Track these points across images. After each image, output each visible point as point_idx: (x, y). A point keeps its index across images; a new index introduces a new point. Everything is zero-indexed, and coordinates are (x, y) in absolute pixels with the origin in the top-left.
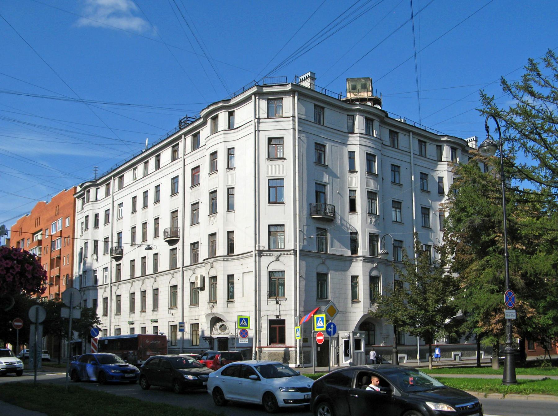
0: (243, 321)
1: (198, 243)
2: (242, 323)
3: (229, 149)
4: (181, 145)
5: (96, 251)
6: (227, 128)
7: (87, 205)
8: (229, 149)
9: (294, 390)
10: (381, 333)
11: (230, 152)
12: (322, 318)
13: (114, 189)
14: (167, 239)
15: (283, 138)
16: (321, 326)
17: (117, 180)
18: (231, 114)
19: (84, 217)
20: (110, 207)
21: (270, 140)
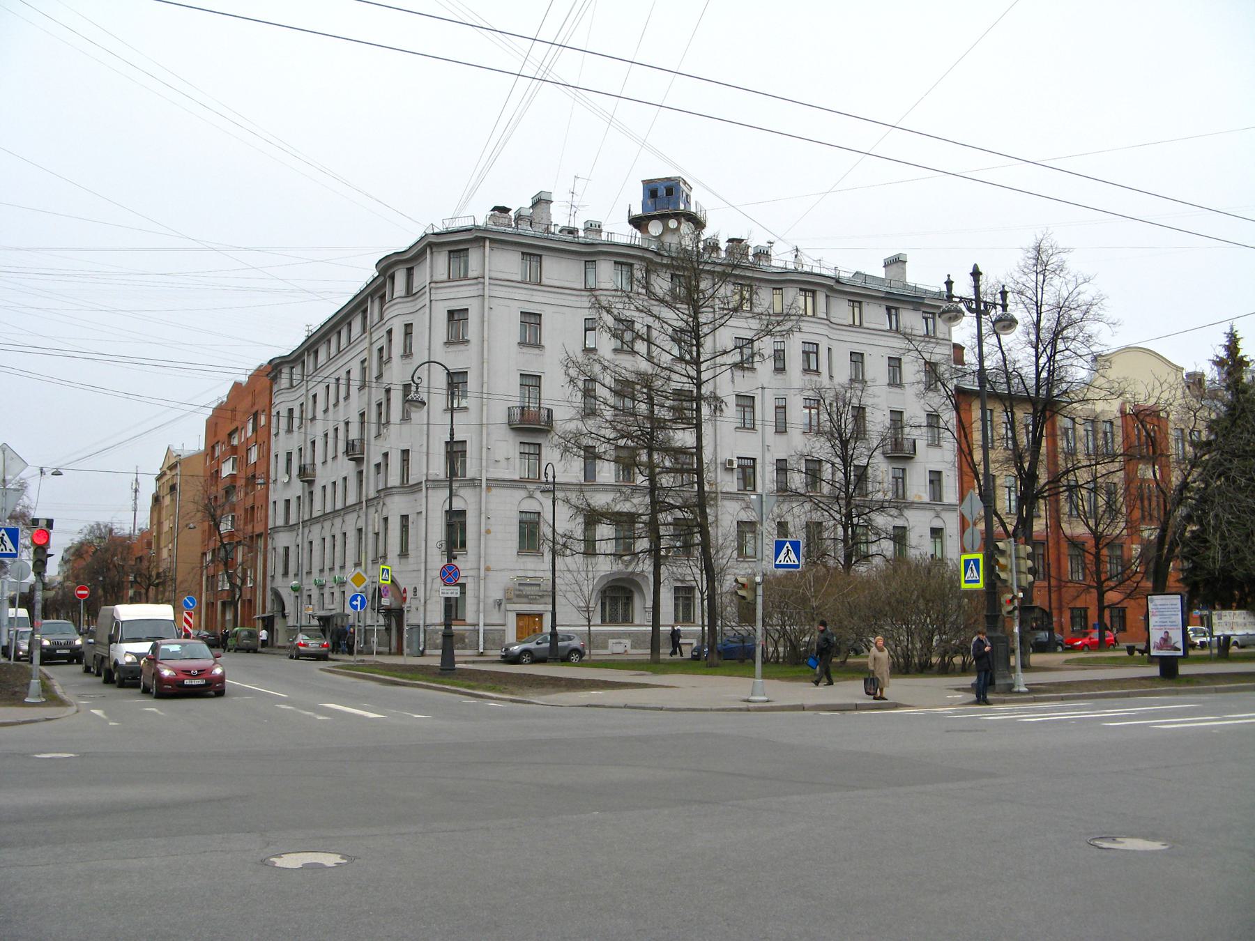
0: (785, 550)
2: (782, 556)
7: (400, 303)
9: (58, 652)
10: (313, 617)
12: (976, 561)
15: (467, 310)
16: (974, 579)
18: (410, 272)
21: (451, 313)
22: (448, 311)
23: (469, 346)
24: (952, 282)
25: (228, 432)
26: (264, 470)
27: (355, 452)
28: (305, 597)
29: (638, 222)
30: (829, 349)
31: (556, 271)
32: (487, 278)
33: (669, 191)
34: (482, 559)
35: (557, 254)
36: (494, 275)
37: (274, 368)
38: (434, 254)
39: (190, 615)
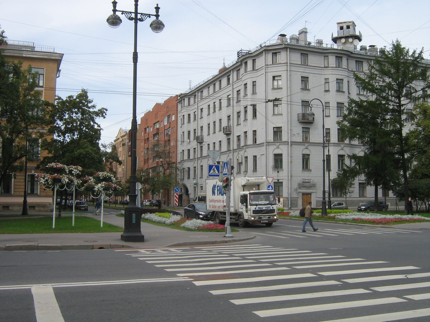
1: (240, 135)
2: (212, 171)
3: (253, 82)
4: (231, 77)
5: (189, 137)
6: (252, 69)
8: (253, 82)
11: (254, 84)
13: (233, 80)
14: (224, 133)
17: (235, 73)
18: (254, 61)
19: (243, 85)
20: (196, 110)
22: (273, 76)
24: (159, 8)
25: (154, 123)
26: (175, 137)
27: (228, 132)
28: (199, 188)
29: (335, 40)
30: (348, 81)
31: (313, 60)
33: (348, 27)
34: (289, 173)
35: (315, 54)
36: (292, 62)
37: (181, 98)
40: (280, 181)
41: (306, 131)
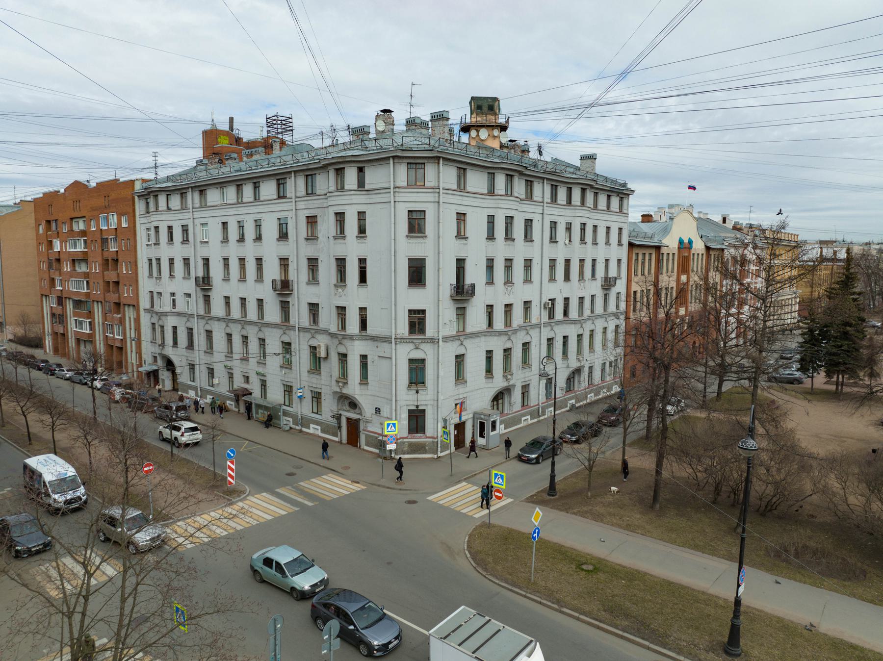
23: (426, 240)
32: (441, 188)
35: (474, 168)
38: (396, 164)
39: (232, 462)
40: (420, 408)
41: (461, 313)
